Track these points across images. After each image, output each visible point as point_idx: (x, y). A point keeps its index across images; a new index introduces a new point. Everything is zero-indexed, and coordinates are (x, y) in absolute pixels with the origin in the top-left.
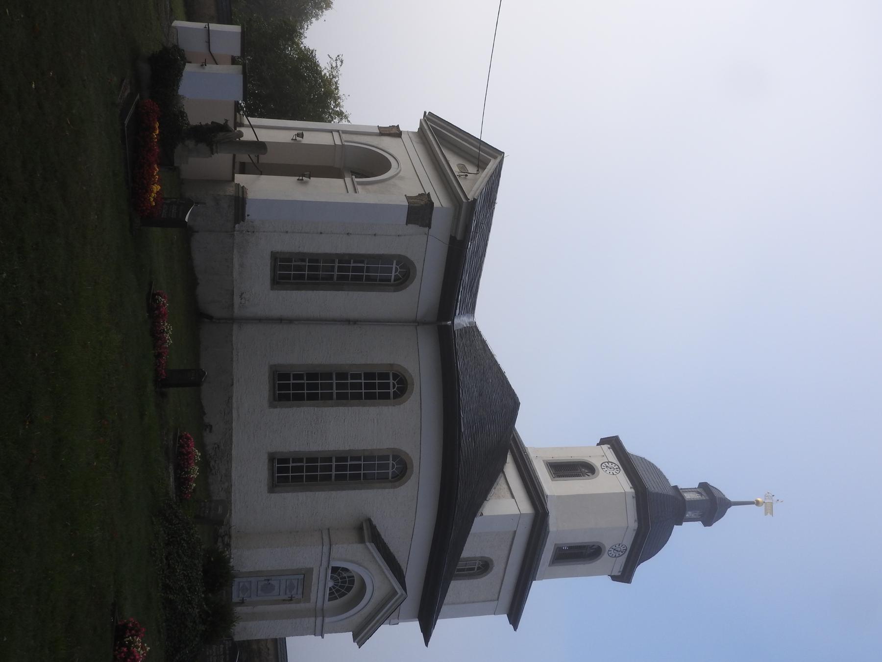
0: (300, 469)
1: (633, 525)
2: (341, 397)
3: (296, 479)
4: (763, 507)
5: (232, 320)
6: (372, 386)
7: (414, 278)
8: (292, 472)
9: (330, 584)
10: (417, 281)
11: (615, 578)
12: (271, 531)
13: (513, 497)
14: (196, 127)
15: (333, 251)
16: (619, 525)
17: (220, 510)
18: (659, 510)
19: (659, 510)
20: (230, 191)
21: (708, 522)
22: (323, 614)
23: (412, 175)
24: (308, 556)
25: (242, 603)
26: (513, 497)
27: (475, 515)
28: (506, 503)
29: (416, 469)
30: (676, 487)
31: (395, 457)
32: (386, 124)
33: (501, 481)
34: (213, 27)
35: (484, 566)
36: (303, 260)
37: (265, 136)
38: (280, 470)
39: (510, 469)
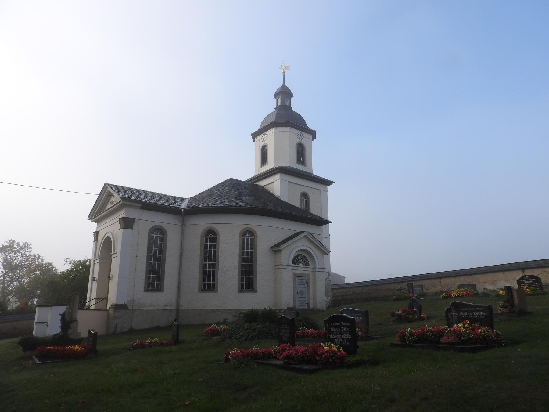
0: (247, 279)
1: (288, 129)
2: (252, 260)
3: (252, 280)
4: (286, 71)
5: (178, 310)
6: (211, 245)
7: (158, 226)
8: (247, 282)
9: (301, 265)
10: (163, 225)
11: (314, 138)
12: (275, 291)
13: (273, 182)
14: (62, 329)
15: (145, 263)
16: (289, 135)
17: (242, 315)
18: (285, 117)
19: (285, 117)
20: (111, 311)
21: (291, 95)
22: (314, 268)
23: (112, 227)
24: (287, 275)
25: (308, 304)
26: (273, 182)
27: (280, 200)
28: (276, 186)
29: (249, 226)
30: (275, 109)
31: (243, 235)
32: (92, 238)
33: (267, 187)
34: (36, 321)
35: (304, 196)
36: (149, 277)
37: (94, 296)
38: (247, 287)
39: (262, 183)
